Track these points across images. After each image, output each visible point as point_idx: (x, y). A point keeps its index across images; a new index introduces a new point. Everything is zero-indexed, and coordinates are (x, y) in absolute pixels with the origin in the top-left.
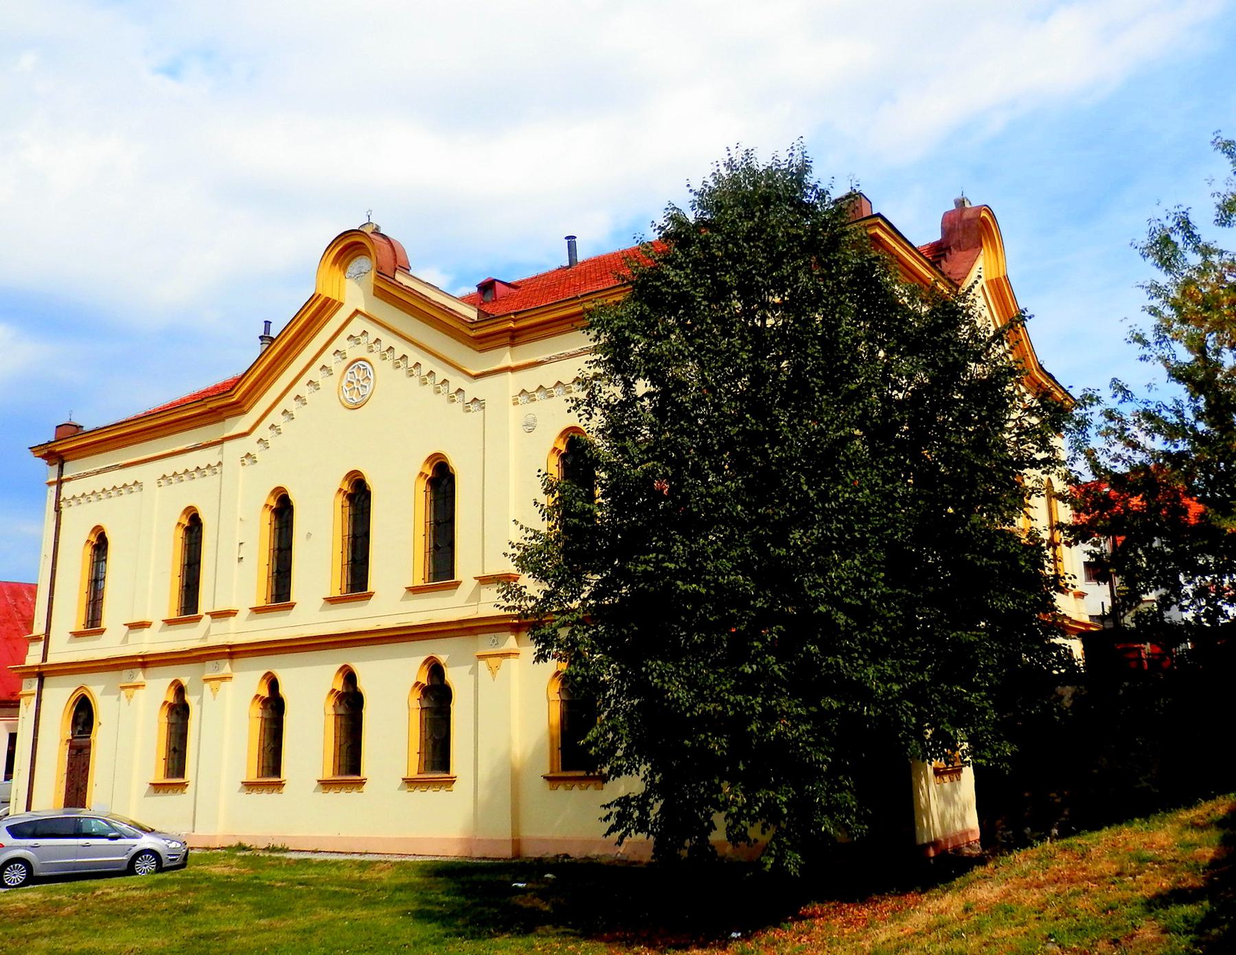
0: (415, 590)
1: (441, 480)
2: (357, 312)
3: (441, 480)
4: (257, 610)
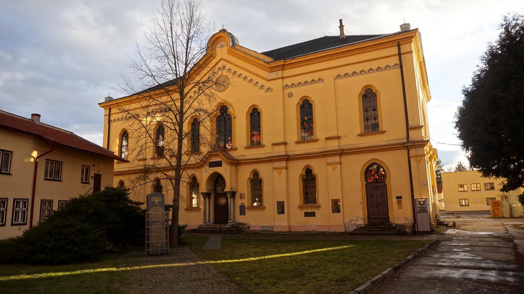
0: (360, 135)
1: (255, 115)
2: (221, 59)
3: (255, 115)
4: (297, 143)
